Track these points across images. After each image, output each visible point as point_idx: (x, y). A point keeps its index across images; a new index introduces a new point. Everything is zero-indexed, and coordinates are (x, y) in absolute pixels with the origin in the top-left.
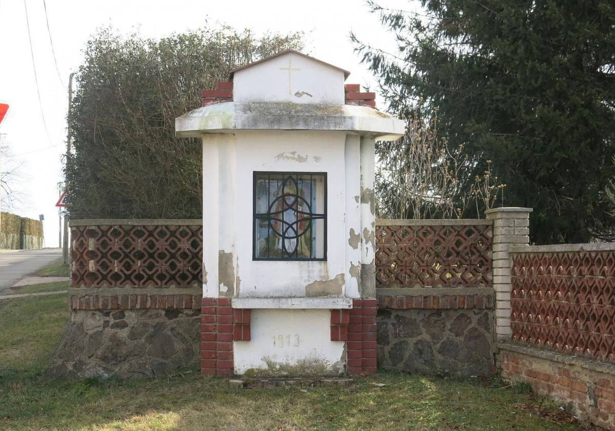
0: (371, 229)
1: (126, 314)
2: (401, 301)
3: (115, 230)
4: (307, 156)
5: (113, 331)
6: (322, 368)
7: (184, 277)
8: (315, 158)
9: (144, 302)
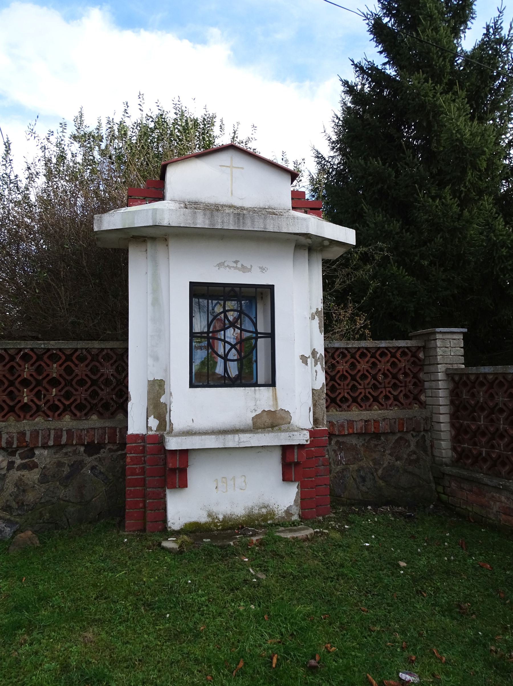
0: (321, 351)
1: (37, 452)
2: (342, 426)
3: (26, 354)
4: (251, 266)
5: (19, 473)
6: (271, 514)
7: (106, 406)
8: (260, 268)
9: (58, 437)
